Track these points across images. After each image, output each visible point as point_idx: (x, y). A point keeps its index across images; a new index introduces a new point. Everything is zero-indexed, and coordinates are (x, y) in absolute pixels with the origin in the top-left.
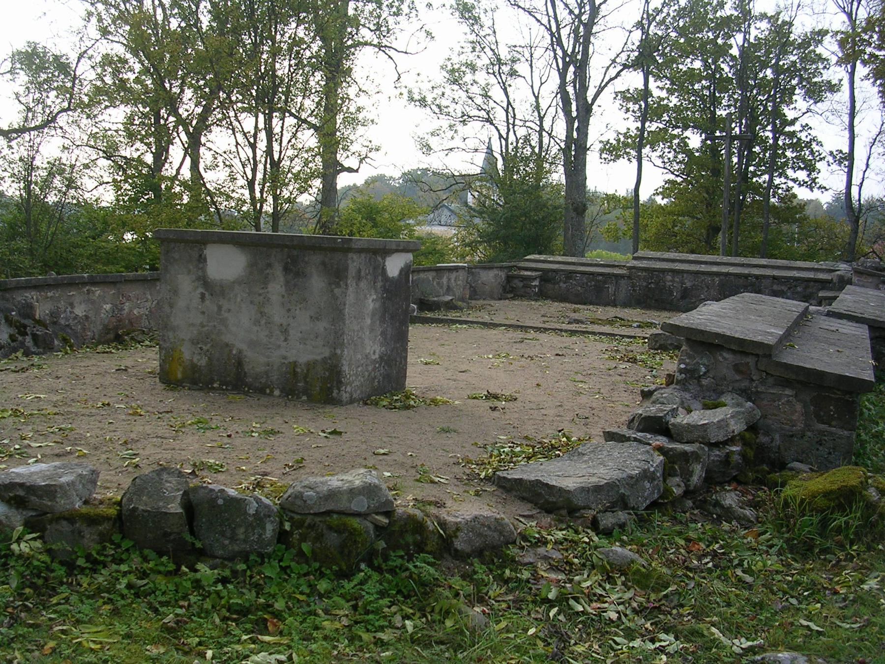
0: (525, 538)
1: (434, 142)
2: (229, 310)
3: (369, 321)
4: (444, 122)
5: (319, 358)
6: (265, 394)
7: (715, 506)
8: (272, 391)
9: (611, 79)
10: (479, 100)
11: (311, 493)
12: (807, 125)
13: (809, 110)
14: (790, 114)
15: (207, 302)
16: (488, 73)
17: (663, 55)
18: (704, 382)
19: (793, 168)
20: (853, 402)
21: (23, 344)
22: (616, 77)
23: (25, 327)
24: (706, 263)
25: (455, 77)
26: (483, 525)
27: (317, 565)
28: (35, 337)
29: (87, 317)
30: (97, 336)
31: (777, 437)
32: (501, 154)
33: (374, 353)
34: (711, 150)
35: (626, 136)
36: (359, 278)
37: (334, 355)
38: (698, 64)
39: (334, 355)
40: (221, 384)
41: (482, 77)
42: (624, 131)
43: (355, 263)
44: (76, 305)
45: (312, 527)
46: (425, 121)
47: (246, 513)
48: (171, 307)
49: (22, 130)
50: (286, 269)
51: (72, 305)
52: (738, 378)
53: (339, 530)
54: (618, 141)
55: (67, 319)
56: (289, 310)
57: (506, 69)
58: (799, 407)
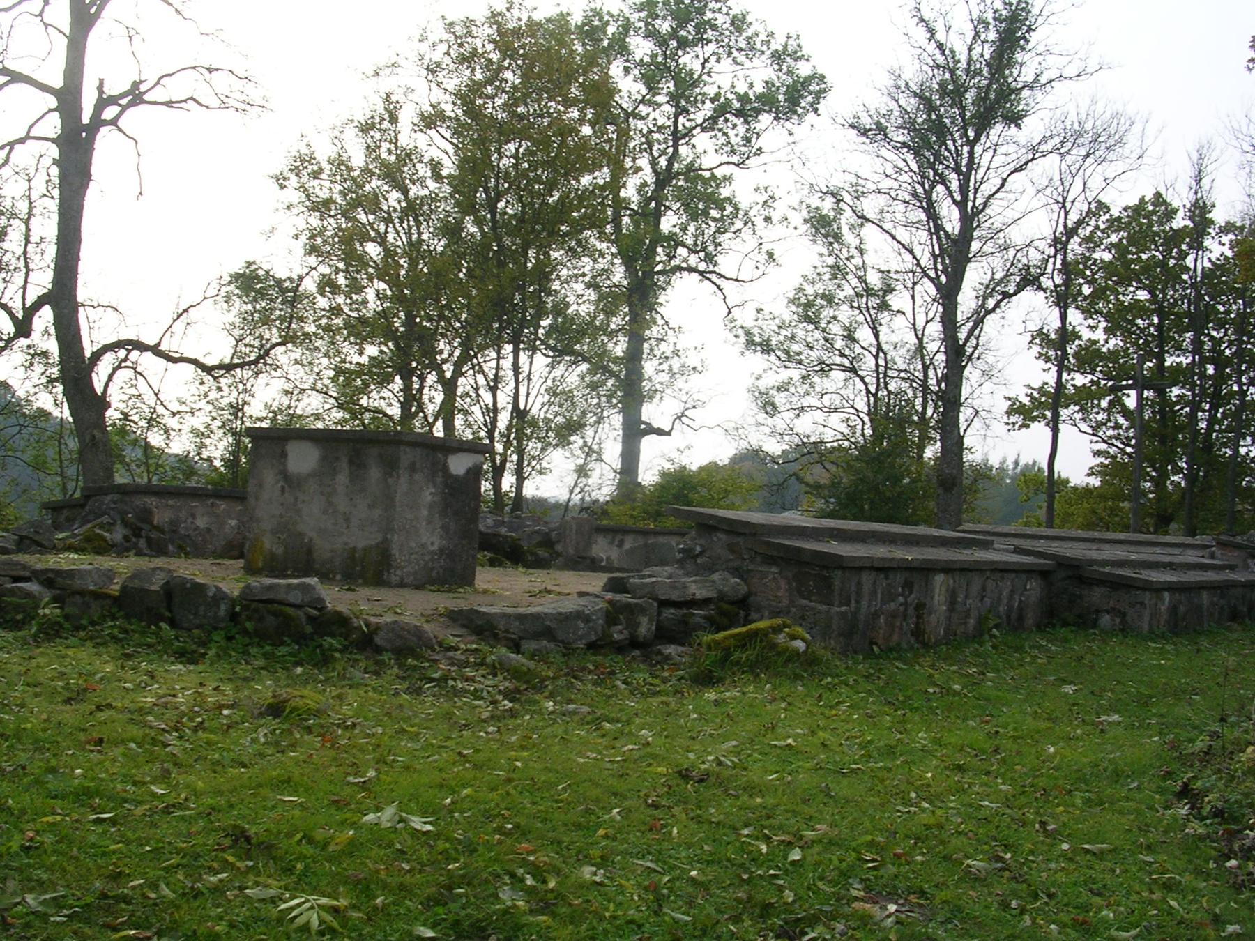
1: (780, 399)
3: (425, 513)
4: (795, 373)
6: (329, 579)
10: (839, 344)
15: (286, 495)
16: (852, 307)
17: (1091, 282)
18: (699, 561)
21: (135, 546)
23: (141, 529)
25: (808, 311)
26: (403, 629)
27: (257, 640)
28: (149, 541)
29: (209, 530)
36: (412, 469)
37: (385, 540)
38: (1143, 295)
39: (385, 540)
41: (845, 313)
45: (256, 610)
46: (771, 372)
47: (206, 595)
48: (257, 500)
49: (228, 368)
50: (351, 462)
51: (193, 516)
53: (276, 614)
57: (873, 302)
58: (783, 584)
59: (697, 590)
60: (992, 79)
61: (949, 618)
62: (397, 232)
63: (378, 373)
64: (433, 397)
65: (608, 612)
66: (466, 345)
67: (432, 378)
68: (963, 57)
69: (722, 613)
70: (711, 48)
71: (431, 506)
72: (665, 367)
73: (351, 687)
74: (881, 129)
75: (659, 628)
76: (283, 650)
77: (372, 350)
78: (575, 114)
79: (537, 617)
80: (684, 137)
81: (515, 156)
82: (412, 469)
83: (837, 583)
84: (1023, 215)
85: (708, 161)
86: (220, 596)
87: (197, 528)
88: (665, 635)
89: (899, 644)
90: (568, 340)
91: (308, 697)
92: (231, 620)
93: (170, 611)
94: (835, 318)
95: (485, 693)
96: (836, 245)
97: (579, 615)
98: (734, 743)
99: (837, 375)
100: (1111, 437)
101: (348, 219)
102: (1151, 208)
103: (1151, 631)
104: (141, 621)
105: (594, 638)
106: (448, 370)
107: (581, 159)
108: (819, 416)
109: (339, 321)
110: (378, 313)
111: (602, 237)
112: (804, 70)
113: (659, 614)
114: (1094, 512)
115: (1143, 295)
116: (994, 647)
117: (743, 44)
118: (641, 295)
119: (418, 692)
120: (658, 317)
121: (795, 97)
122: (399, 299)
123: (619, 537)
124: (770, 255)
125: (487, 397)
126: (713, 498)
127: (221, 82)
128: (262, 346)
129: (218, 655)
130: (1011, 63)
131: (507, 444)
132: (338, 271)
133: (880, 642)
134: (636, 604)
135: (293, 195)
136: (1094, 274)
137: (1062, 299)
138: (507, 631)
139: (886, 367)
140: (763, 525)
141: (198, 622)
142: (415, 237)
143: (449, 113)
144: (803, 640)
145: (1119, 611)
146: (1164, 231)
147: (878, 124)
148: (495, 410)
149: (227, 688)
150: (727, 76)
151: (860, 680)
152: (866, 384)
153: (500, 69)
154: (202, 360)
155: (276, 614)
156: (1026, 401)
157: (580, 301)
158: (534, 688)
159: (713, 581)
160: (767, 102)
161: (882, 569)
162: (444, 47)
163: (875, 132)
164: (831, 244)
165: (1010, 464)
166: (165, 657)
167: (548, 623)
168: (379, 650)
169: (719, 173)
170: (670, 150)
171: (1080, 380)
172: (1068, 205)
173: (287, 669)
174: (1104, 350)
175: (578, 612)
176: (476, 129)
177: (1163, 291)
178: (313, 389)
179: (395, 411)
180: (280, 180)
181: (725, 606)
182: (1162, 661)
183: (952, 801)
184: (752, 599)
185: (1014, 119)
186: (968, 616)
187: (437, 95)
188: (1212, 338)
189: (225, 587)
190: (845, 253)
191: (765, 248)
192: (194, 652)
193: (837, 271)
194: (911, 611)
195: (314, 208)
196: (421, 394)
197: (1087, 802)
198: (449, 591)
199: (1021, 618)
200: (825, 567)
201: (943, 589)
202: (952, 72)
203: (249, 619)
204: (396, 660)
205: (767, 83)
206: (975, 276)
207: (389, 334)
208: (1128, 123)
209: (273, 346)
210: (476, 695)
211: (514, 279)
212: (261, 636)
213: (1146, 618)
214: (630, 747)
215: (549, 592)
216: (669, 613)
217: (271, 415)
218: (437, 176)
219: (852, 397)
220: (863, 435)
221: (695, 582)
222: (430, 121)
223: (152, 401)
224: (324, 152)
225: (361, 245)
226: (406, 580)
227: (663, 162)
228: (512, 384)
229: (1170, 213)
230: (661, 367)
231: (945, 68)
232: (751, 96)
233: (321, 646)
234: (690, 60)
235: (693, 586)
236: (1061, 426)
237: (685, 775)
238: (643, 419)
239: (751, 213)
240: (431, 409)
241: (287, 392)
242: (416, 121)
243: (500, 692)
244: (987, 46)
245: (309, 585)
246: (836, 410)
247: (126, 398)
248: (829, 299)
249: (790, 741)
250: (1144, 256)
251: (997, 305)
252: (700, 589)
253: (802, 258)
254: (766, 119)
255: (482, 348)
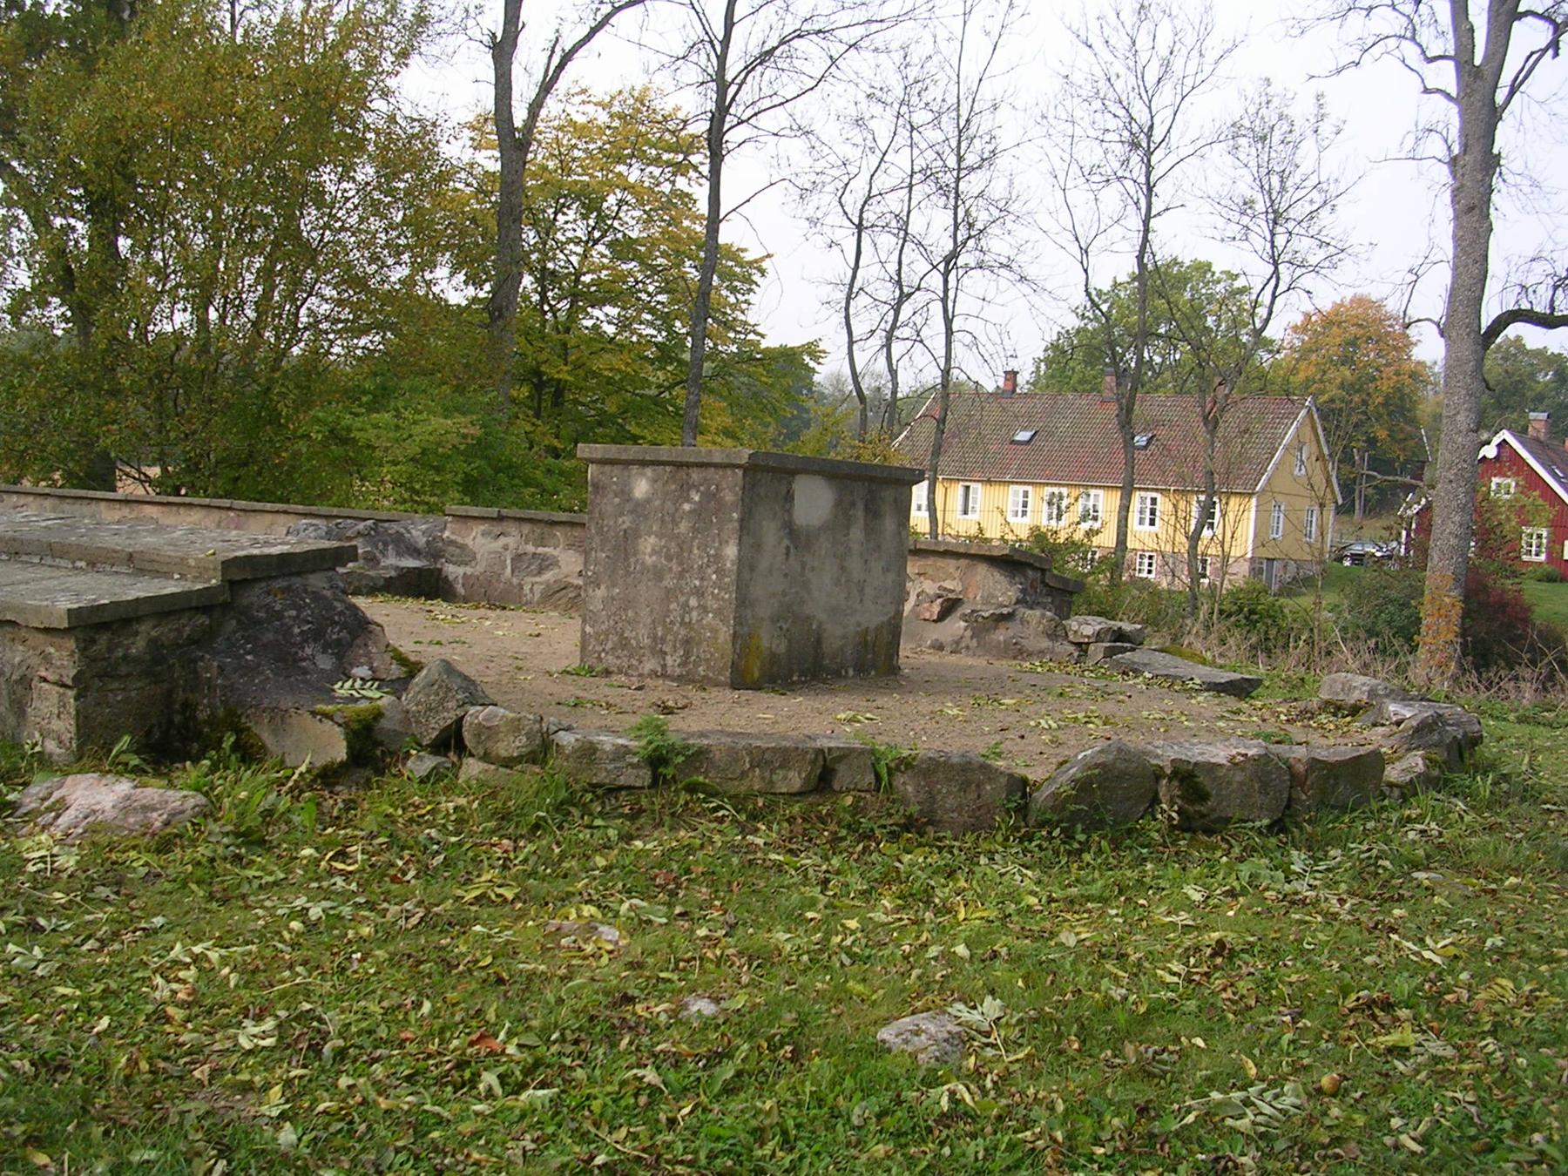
15: (792, 558)
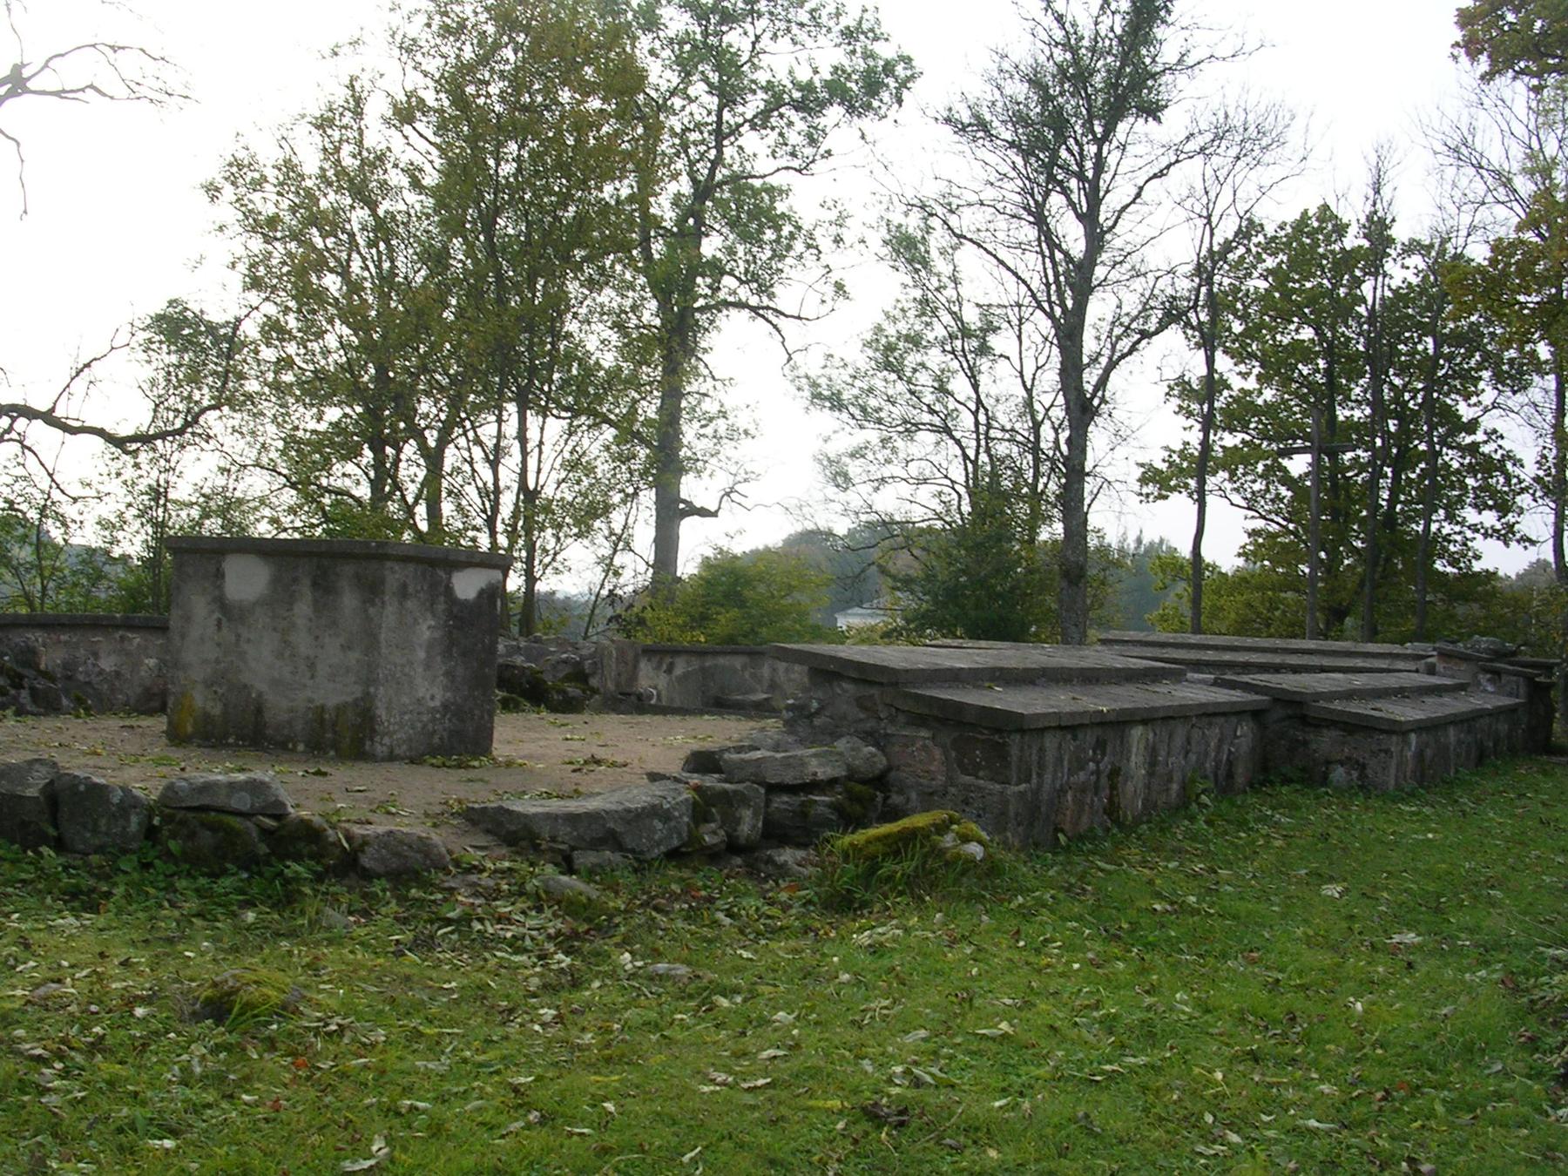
0: (457, 863)
1: (854, 468)
2: (249, 641)
3: (422, 655)
4: (872, 435)
5: (350, 699)
7: (767, 863)
8: (295, 746)
9: (1123, 356)
10: (929, 398)
11: (184, 784)
12: (1495, 431)
13: (1495, 405)
14: (1466, 412)
15: (225, 630)
17: (1244, 318)
18: (817, 722)
19: (1475, 506)
20: (1004, 744)
22: (1130, 352)
24: (1215, 648)
25: (889, 357)
26: (402, 842)
28: (34, 693)
29: (118, 674)
30: (132, 701)
31: (914, 796)
32: (967, 486)
33: (433, 698)
34: (1329, 478)
35: (1182, 454)
36: (403, 593)
37: (368, 697)
38: (1307, 333)
40: (237, 739)
41: (935, 358)
42: (1178, 446)
43: (395, 575)
44: (102, 654)
45: (183, 823)
46: (842, 434)
47: (108, 801)
49: (145, 439)
51: (96, 655)
52: (862, 716)
53: (213, 828)
54: (1171, 464)
55: (87, 674)
56: (317, 638)
58: (937, 753)
59: (822, 770)
60: (1125, 58)
61: (1148, 787)
62: (364, 259)
63: (340, 444)
64: (412, 471)
65: (695, 804)
66: (456, 403)
67: (410, 449)
68: (1087, 31)
69: (852, 797)
70: (762, 23)
71: (430, 646)
72: (709, 431)
73: (330, 942)
74: (983, 126)
75: (767, 823)
76: (226, 882)
77: (333, 414)
78: (595, 104)
79: (594, 817)
80: (732, 133)
81: (518, 159)
82: (403, 593)
83: (1014, 752)
84: (1160, 237)
85: (763, 165)
86: (130, 803)
87: (101, 672)
88: (776, 833)
89: (1091, 829)
90: (586, 397)
91: (264, 974)
92: (147, 838)
93: (56, 827)
94: (923, 365)
95: (528, 942)
96: (923, 273)
97: (653, 811)
98: (922, 1033)
99: (926, 438)
100: (1270, 512)
101: (301, 243)
102: (1316, 224)
103: (1398, 787)
104: (13, 843)
105: (676, 843)
106: (431, 438)
107: (604, 164)
108: (905, 489)
109: (288, 377)
110: (341, 366)
111: (630, 263)
112: (885, 51)
113: (768, 803)
114: (1249, 605)
115: (1307, 333)
116: (1209, 823)
117: (803, 16)
118: (676, 342)
119: (425, 944)
120: (701, 366)
121: (869, 86)
122: (367, 347)
123: (668, 660)
124: (839, 287)
125: (486, 473)
126: (773, 596)
127: (130, 64)
128: (189, 411)
129: (128, 897)
130: (1148, 41)
131: (512, 534)
132: (287, 310)
133: (1067, 827)
134: (735, 792)
135: (226, 212)
136: (1246, 308)
137: (1209, 341)
138: (553, 839)
139: (989, 426)
140: (907, 671)
141: (97, 842)
142: (386, 265)
143: (431, 102)
144: (980, 842)
145: (1357, 762)
146: (1332, 252)
147: (977, 116)
148: (497, 491)
149: (141, 959)
150: (783, 61)
151: (1061, 896)
152: (962, 449)
153: (497, 46)
154: (109, 429)
155: (213, 828)
156: (1164, 467)
157: (598, 343)
158: (599, 928)
159: (841, 754)
160: (837, 90)
161: (1069, 727)
162: (423, 19)
163: (976, 128)
164: (917, 271)
165: (1131, 545)
166: (49, 900)
167: (611, 825)
168: (368, 875)
169: (774, 181)
170: (713, 152)
171: (1231, 440)
172: (1214, 220)
173: (234, 915)
174: (1260, 402)
175: (653, 806)
176: (467, 124)
177: (1333, 329)
178: (257, 465)
179: (364, 491)
180: (212, 191)
181: (858, 788)
182: (1421, 833)
183: (1268, 1126)
184: (893, 774)
185: (1152, 111)
186: (1170, 780)
187: (415, 80)
188: (1393, 387)
189: (137, 789)
190: (935, 282)
191: (834, 277)
192: (93, 890)
193: (926, 307)
194: (1104, 781)
195: (255, 228)
196: (397, 469)
197: (1452, 1107)
198: (459, 767)
199: (1230, 775)
200: (998, 731)
201: (1142, 746)
202: (1074, 51)
203: (174, 836)
204: (394, 889)
205: (836, 68)
206: (1099, 309)
207: (355, 393)
208: (1288, 116)
209: (203, 411)
210: (516, 945)
211: (519, 319)
212: (194, 862)
213: (1393, 771)
214: (771, 1052)
215: (598, 762)
216: (782, 801)
217: (202, 500)
218: (416, 184)
219: (945, 465)
220: (961, 513)
221: (815, 755)
222: (405, 114)
223: (45, 483)
224: (268, 156)
225: (319, 278)
226: (397, 751)
227: (703, 169)
228: (517, 457)
229: (1341, 230)
230: (702, 431)
231: (1066, 46)
232: (818, 84)
233: (281, 874)
234: (736, 39)
235: (814, 762)
236: (1209, 499)
237: (873, 1115)
238: (683, 496)
239: (817, 234)
240: (411, 491)
241: (223, 470)
242: (389, 113)
243: (549, 937)
244: (1118, 18)
245: (263, 783)
246: (925, 481)
247: (10, 480)
248: (915, 341)
249: (1004, 1026)
250: (1308, 285)
251: (1133, 349)
252: (821, 765)
253: (882, 290)
254: (835, 112)
255: (478, 409)
